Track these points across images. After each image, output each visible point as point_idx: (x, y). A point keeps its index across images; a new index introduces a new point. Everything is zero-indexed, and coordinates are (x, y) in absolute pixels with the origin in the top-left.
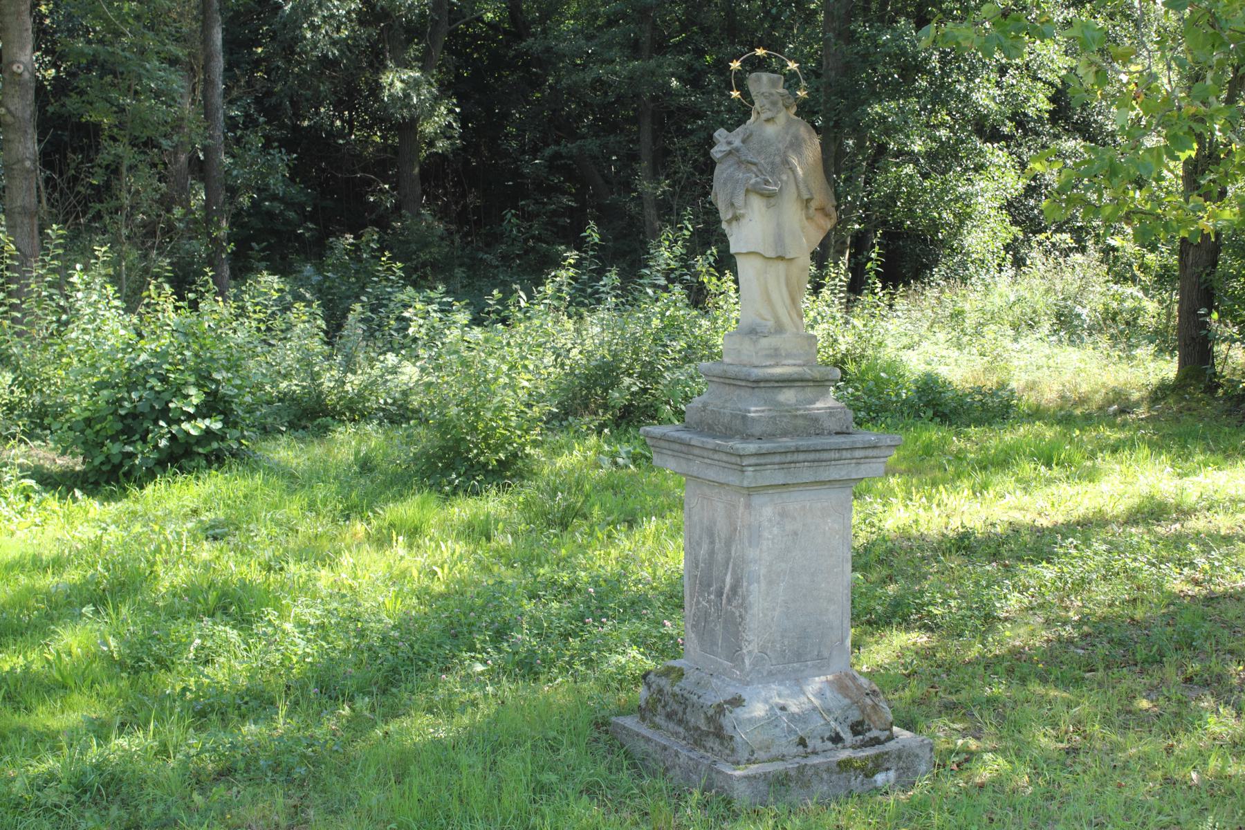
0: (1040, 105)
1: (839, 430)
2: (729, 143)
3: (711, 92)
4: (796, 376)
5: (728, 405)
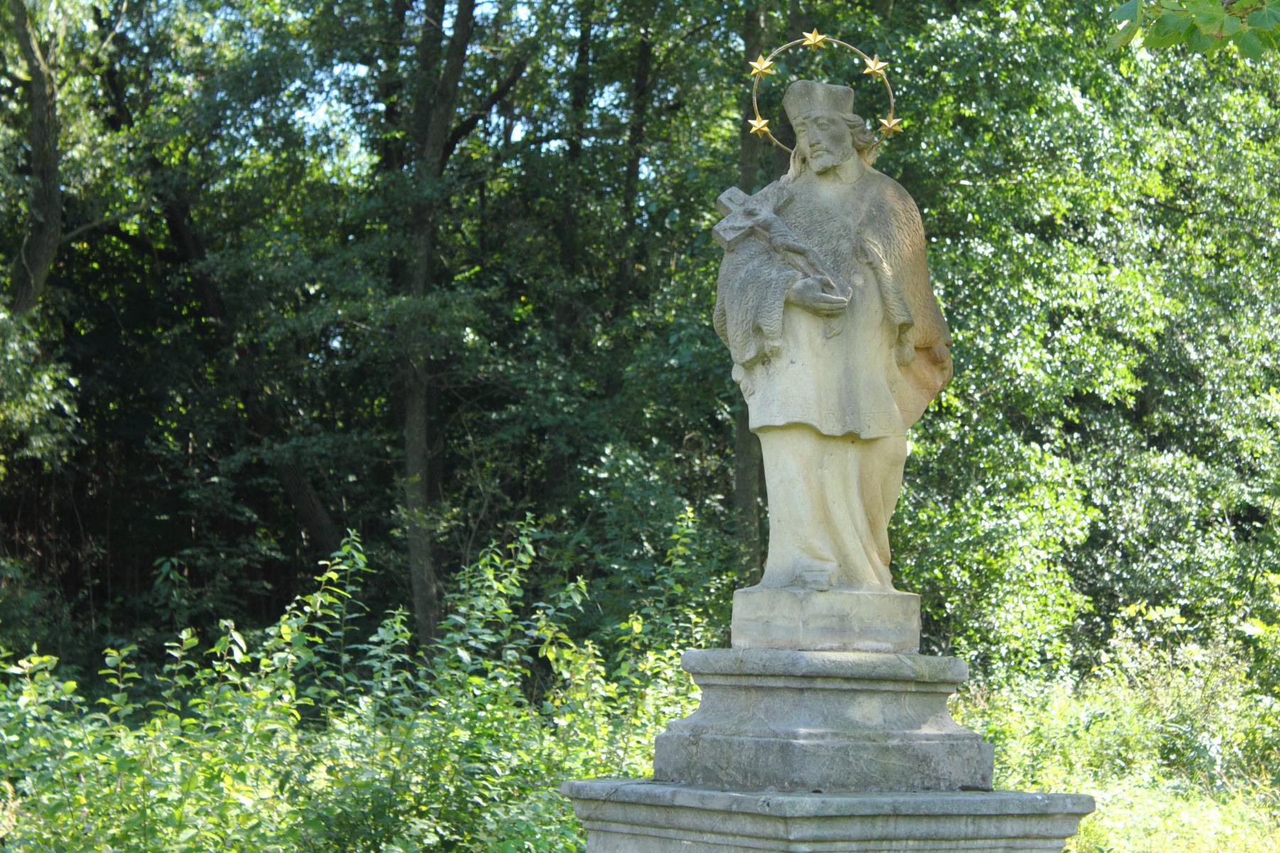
0: (1119, 383)
1: (968, 781)
2: (750, 214)
3: (533, 357)
4: (883, 670)
5: (748, 727)
